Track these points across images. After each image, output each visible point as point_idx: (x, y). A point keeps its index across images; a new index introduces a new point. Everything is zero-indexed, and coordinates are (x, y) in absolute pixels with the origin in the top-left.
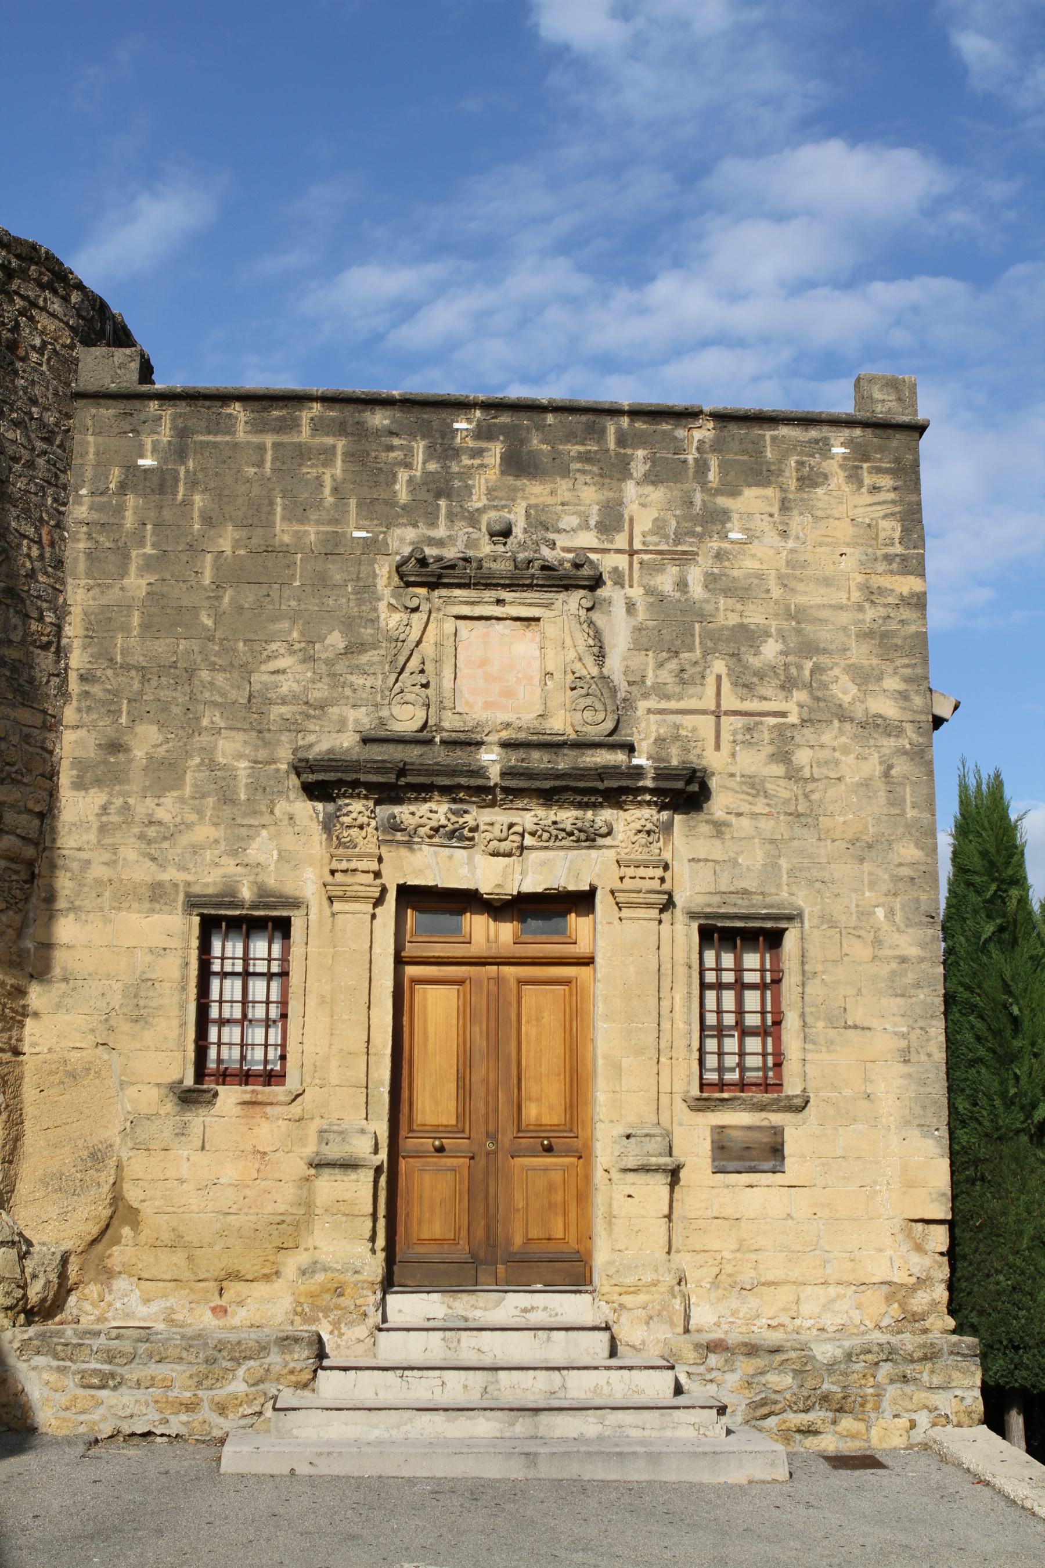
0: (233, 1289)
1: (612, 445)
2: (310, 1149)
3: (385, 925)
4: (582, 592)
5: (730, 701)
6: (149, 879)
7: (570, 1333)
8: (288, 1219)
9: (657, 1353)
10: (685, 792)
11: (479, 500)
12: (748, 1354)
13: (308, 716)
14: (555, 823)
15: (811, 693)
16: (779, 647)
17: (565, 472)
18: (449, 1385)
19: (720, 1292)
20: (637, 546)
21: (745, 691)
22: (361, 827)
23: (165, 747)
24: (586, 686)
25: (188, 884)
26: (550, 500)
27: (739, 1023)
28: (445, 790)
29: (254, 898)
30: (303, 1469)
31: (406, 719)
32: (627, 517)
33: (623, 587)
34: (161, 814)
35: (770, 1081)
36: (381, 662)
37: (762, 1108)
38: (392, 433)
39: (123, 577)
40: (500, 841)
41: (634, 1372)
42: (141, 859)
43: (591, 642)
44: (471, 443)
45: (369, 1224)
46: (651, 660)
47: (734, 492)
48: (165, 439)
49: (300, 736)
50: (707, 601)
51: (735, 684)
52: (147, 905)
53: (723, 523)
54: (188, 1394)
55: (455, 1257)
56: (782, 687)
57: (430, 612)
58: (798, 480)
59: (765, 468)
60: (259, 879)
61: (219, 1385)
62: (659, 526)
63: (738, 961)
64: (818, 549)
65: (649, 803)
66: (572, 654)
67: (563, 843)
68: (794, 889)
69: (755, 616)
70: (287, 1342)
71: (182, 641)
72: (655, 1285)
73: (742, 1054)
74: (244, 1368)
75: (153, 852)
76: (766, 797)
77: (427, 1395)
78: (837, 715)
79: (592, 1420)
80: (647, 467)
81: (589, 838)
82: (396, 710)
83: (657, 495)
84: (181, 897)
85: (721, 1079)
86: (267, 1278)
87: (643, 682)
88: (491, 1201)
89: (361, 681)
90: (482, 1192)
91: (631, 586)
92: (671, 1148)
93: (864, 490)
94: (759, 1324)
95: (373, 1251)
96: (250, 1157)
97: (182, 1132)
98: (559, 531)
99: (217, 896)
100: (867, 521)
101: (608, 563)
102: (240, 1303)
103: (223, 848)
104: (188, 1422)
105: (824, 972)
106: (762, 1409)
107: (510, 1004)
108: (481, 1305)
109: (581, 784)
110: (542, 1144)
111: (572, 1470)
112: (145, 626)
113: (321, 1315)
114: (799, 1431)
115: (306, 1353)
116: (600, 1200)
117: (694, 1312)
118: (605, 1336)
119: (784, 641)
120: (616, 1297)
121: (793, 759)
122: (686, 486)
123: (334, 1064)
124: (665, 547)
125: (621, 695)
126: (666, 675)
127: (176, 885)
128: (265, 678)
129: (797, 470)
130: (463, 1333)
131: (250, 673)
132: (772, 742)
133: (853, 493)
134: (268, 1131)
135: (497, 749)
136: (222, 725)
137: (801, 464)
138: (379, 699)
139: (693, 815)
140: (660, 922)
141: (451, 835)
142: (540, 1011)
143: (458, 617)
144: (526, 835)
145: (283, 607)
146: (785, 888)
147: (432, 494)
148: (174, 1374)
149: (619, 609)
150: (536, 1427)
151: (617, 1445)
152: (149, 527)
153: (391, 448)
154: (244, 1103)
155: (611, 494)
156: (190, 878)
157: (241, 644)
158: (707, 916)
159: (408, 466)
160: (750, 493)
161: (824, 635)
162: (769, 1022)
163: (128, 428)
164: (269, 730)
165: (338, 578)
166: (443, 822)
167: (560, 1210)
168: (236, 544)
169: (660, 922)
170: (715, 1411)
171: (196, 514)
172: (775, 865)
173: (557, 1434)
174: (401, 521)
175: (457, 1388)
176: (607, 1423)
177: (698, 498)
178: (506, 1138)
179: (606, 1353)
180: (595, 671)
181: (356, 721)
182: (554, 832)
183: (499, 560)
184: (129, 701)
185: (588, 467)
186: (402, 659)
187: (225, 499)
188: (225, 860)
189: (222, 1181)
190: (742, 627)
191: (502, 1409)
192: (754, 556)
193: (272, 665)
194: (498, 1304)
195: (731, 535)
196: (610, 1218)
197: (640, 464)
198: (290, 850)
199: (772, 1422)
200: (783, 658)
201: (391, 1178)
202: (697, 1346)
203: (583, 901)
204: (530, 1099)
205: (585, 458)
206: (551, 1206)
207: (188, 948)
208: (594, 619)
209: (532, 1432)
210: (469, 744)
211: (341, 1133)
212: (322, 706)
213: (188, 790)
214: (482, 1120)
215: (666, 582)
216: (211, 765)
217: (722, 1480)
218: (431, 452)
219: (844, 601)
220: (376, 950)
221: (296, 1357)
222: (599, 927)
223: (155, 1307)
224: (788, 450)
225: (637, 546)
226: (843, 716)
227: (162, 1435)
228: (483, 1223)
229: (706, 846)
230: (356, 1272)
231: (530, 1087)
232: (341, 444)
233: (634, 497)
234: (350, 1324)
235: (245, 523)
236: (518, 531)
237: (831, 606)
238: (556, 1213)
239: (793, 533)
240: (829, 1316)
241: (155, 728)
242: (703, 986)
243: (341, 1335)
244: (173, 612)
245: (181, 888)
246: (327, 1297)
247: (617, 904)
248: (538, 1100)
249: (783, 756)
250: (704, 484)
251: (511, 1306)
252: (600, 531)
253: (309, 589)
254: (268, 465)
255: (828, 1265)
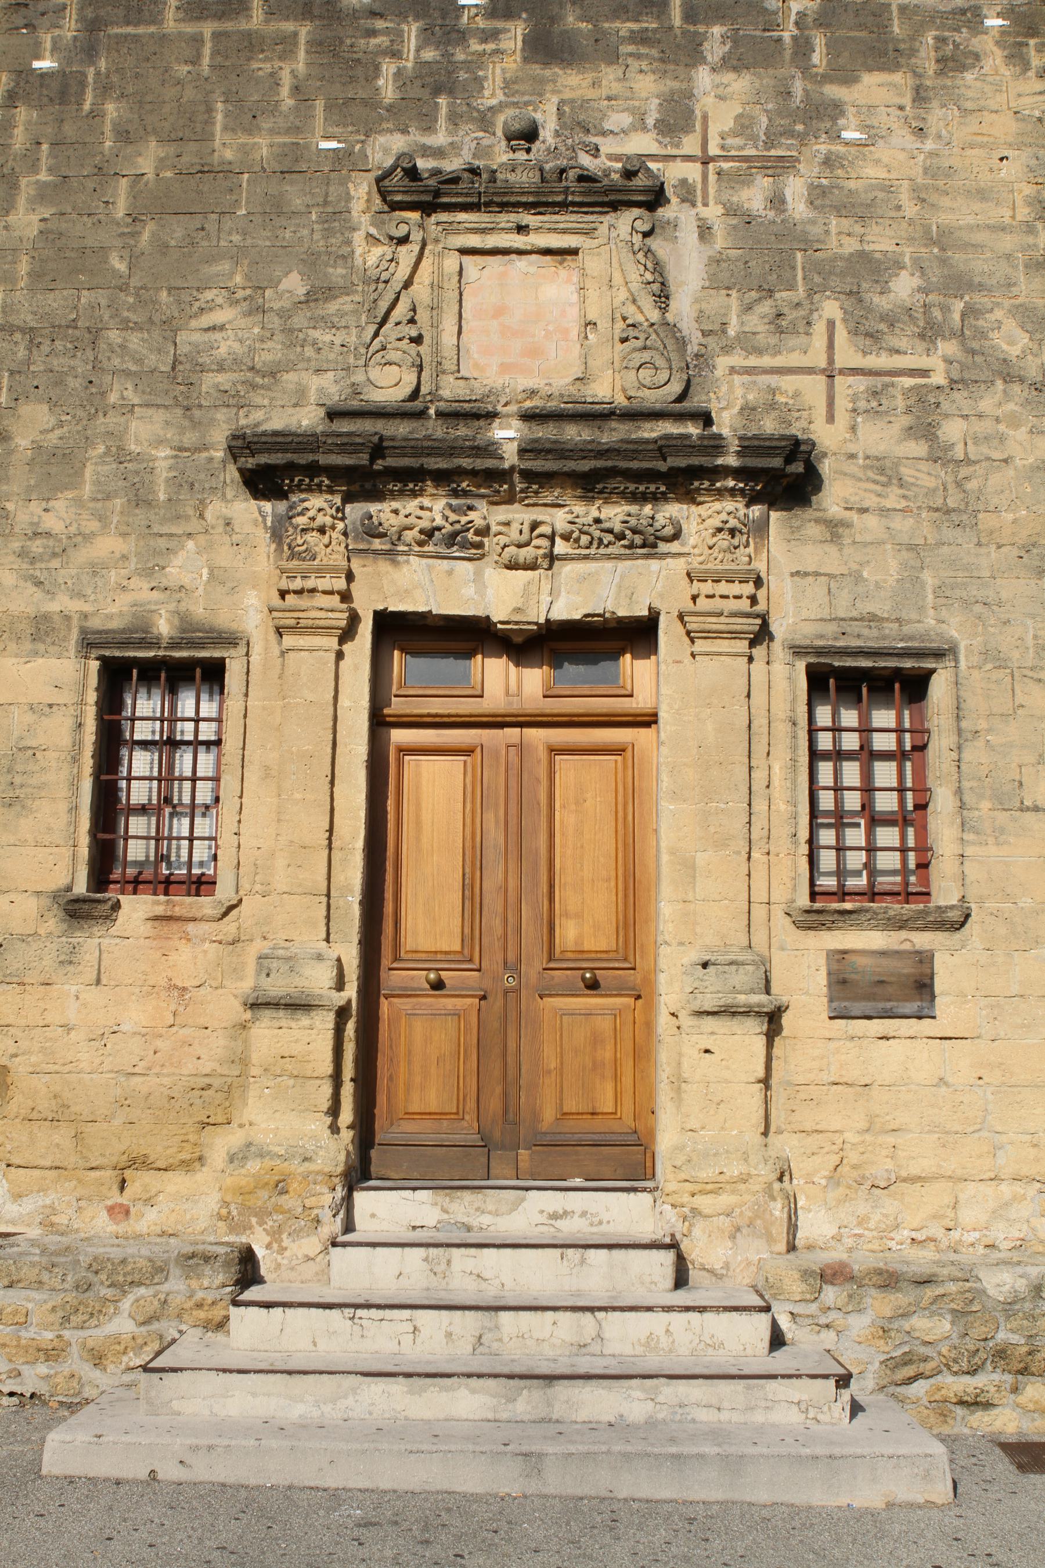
0: (140, 1182)
1: (677, 21)
2: (246, 985)
3: (356, 667)
4: (636, 212)
5: (847, 355)
6: (31, 611)
7: (616, 1253)
8: (216, 1082)
9: (747, 1281)
10: (784, 477)
11: (493, 95)
12: (884, 1287)
13: (254, 387)
14: (597, 521)
15: (963, 344)
16: (916, 281)
17: (613, 57)
18: (424, 1333)
19: (841, 1190)
20: (713, 150)
21: (868, 342)
22: (322, 530)
23: (58, 432)
24: (642, 336)
25: (85, 616)
26: (591, 94)
27: (867, 806)
28: (442, 477)
29: (175, 633)
30: (169, 1472)
31: (389, 385)
32: (698, 113)
33: (694, 205)
34: (52, 523)
35: (912, 889)
36: (355, 312)
37: (901, 924)
38: (374, 14)
39: (7, 213)
40: (519, 546)
41: (707, 1315)
42: (22, 583)
43: (649, 277)
44: (481, 23)
45: (327, 1090)
46: (734, 302)
47: (849, 79)
48: (69, 34)
49: (241, 413)
50: (813, 222)
51: (854, 332)
52: (28, 646)
53: (834, 119)
54: (49, 1335)
55: (458, 1138)
56: (922, 336)
57: (424, 245)
58: (938, 61)
59: (891, 47)
60: (183, 607)
61: (94, 1322)
62: (743, 126)
63: (865, 718)
64: (969, 152)
65: (732, 492)
66: (623, 295)
67: (610, 550)
68: (944, 613)
69: (881, 241)
70: (195, 1260)
71: (85, 293)
72: (745, 1182)
73: (871, 849)
74: (131, 1298)
75: (38, 573)
76: (901, 486)
77: (391, 1347)
78: (1000, 373)
79: (637, 1394)
80: (727, 48)
81: (648, 543)
82: (375, 373)
83: (740, 84)
84: (75, 635)
85: (841, 886)
86: (187, 1165)
87: (724, 332)
88: (510, 1060)
89: (328, 338)
90: (497, 1043)
91: (706, 205)
92: (768, 982)
93: (1031, 74)
94: (898, 1238)
95: (334, 1129)
96: (164, 994)
97: (69, 960)
98: (604, 133)
99: (123, 631)
100: (1037, 113)
101: (673, 173)
102: (149, 1201)
103: (133, 567)
104: (48, 1377)
105: (989, 731)
106: (906, 1368)
107: (538, 781)
108: (491, 1207)
109: (635, 465)
110: (583, 979)
111: (598, 1481)
112: (35, 275)
113: (254, 1220)
114: (961, 1403)
115: (220, 1278)
116: (664, 1056)
117: (804, 1220)
118: (669, 1256)
119: (923, 274)
120: (686, 1199)
121: (939, 433)
122: (782, 72)
123: (280, 862)
124: (753, 152)
125: (692, 348)
126: (755, 322)
127: (68, 618)
128: (197, 337)
129: (937, 49)
130: (454, 1250)
131: (175, 332)
132: (908, 411)
133: (1016, 77)
134: (191, 957)
135: (516, 423)
136: (136, 401)
137: (941, 40)
138: (352, 360)
139: (798, 511)
140: (751, 659)
141: (451, 540)
142: (583, 789)
143: (464, 251)
144: (558, 540)
145: (222, 243)
146: (931, 612)
147: (428, 90)
148: (30, 1306)
149: (688, 234)
150: (549, 1405)
151: (673, 1440)
152: (45, 147)
153: (372, 33)
154: (156, 918)
155: (676, 85)
156: (87, 608)
157: (164, 294)
158: (819, 652)
159: (396, 54)
160: (870, 80)
161: (978, 265)
162: (910, 806)
163: (21, 22)
164: (200, 406)
165: (298, 202)
166: (439, 521)
167: (609, 1073)
168: (161, 164)
169: (751, 659)
170: (832, 1382)
171: (108, 128)
172: (916, 580)
173: (582, 1415)
174: (385, 126)
175: (436, 1337)
176: (661, 1399)
177: (798, 87)
178: (533, 968)
179: (670, 1283)
180: (655, 316)
181: (321, 390)
182: (597, 534)
183: (518, 171)
184: (12, 373)
185: (644, 50)
186: (383, 305)
187: (148, 107)
188: (135, 582)
189: (124, 1028)
190: (863, 256)
191: (496, 1376)
192: (877, 161)
193: (206, 320)
194: (515, 1206)
195: (846, 135)
196: (679, 1082)
197: (716, 45)
198: (225, 569)
199: (920, 1388)
200: (921, 297)
201: (364, 1026)
202: (806, 1274)
203: (639, 634)
204: (567, 915)
205: (641, 38)
206: (596, 1066)
207: (82, 702)
208: (654, 247)
209: (542, 1412)
210: (476, 416)
211: (289, 959)
212: (273, 373)
213: (88, 489)
214: (498, 945)
215: (754, 197)
216: (121, 456)
217: (843, 1501)
218: (427, 36)
219: (1007, 220)
220: (344, 702)
221: (206, 1283)
222: (663, 667)
223: (29, 1205)
224: (922, 24)
225: (713, 150)
226: (1008, 373)
227: (12, 1394)
228: (499, 1090)
229: (815, 554)
230: (305, 1159)
231: (567, 898)
232: (304, 31)
233: (709, 88)
234: (295, 1234)
235: (173, 136)
236: (547, 134)
237: (988, 227)
238: (603, 1076)
239: (933, 130)
240: (1001, 1225)
241: (45, 407)
242: (815, 755)
243: (282, 1250)
244: (73, 255)
245: (75, 622)
246: (264, 1194)
247: (688, 633)
248: (579, 916)
249: (924, 429)
250: (806, 69)
251: (532, 1210)
252: (661, 132)
253: (258, 219)
254: (206, 61)
255: (999, 1153)
